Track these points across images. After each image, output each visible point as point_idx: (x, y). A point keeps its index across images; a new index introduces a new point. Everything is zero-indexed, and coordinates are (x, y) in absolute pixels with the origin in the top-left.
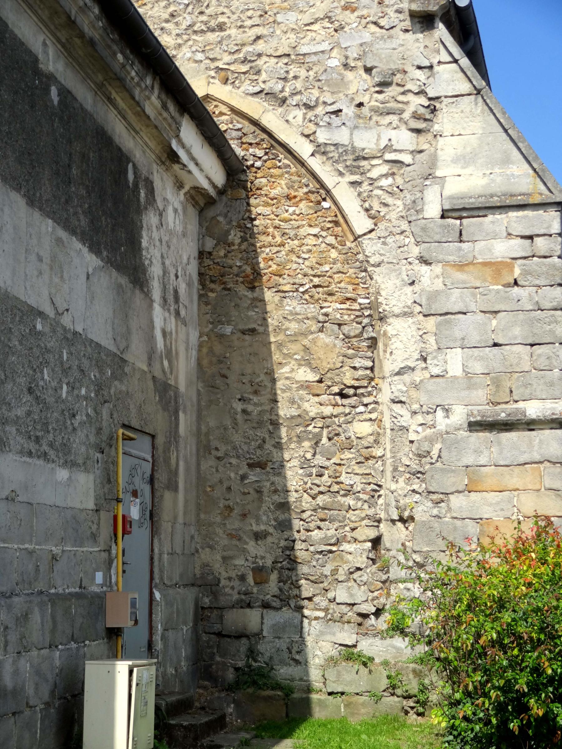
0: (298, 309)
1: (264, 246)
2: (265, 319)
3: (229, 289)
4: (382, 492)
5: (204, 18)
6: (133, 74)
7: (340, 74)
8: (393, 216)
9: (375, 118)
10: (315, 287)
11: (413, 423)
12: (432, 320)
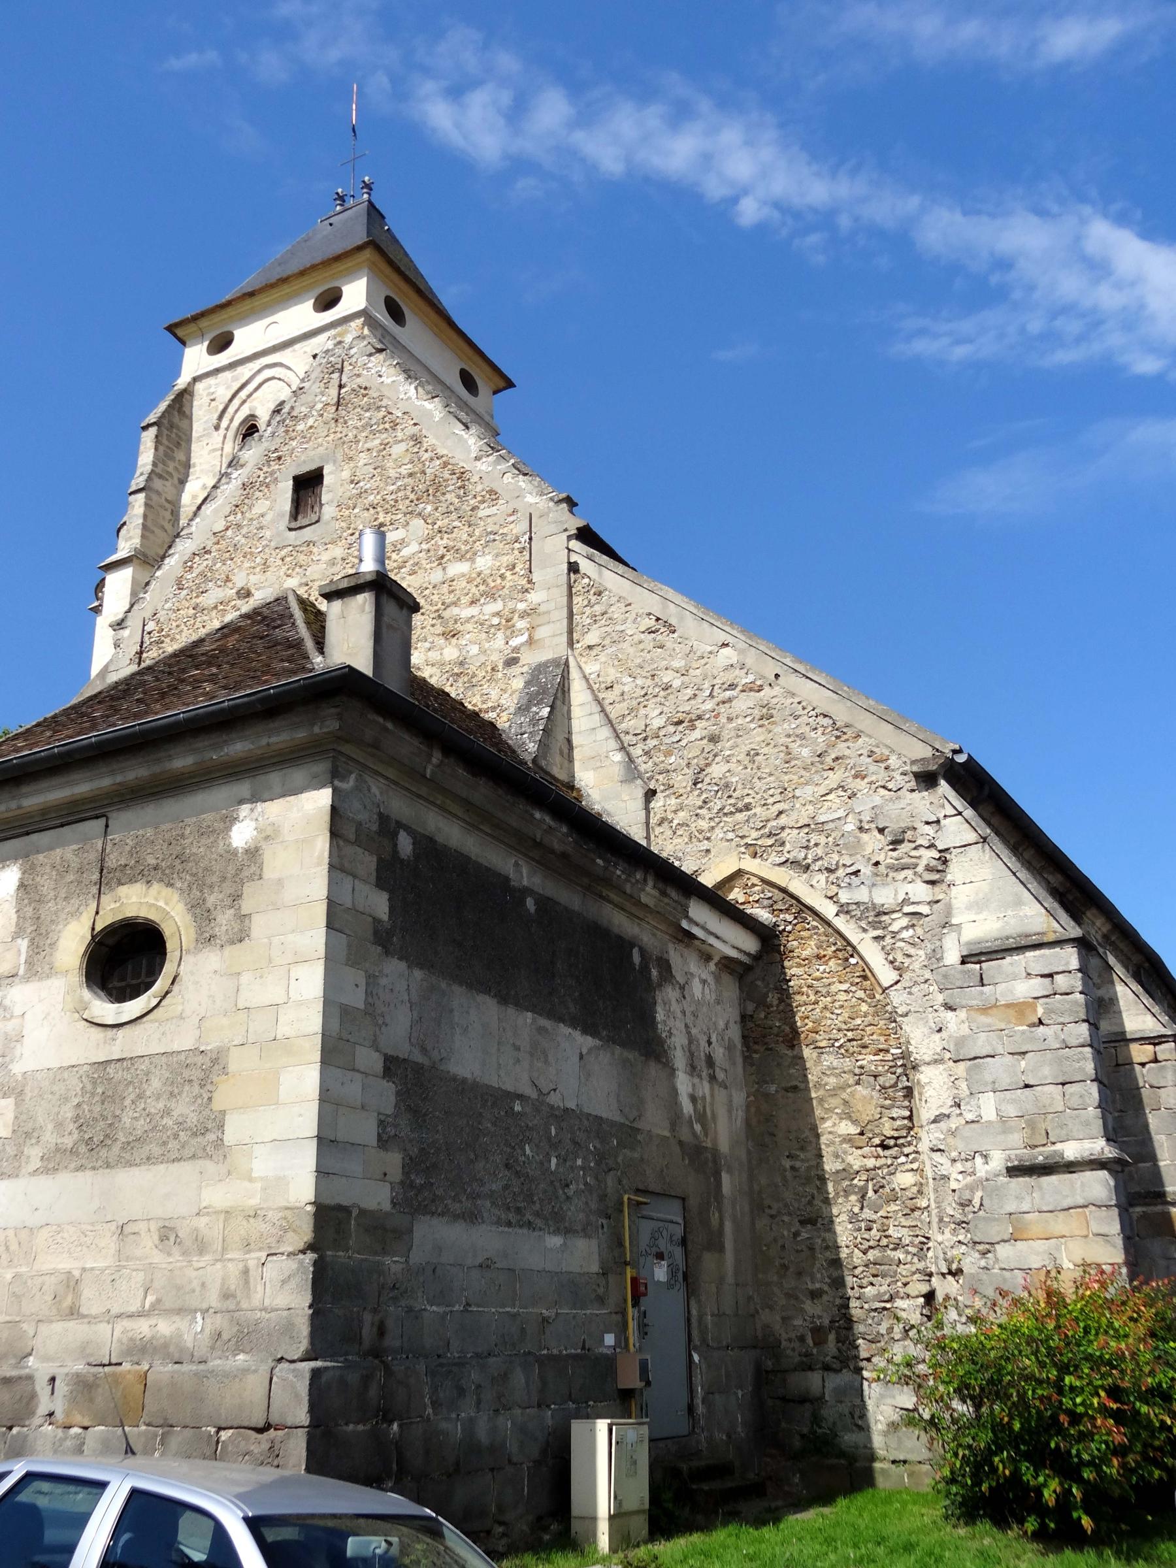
0: (835, 1064)
1: (800, 1005)
2: (805, 1076)
3: (771, 1049)
4: (930, 1244)
5: (732, 801)
6: (618, 872)
7: (856, 837)
8: (916, 966)
9: (891, 874)
10: (849, 1040)
11: (954, 1171)
12: (962, 1066)
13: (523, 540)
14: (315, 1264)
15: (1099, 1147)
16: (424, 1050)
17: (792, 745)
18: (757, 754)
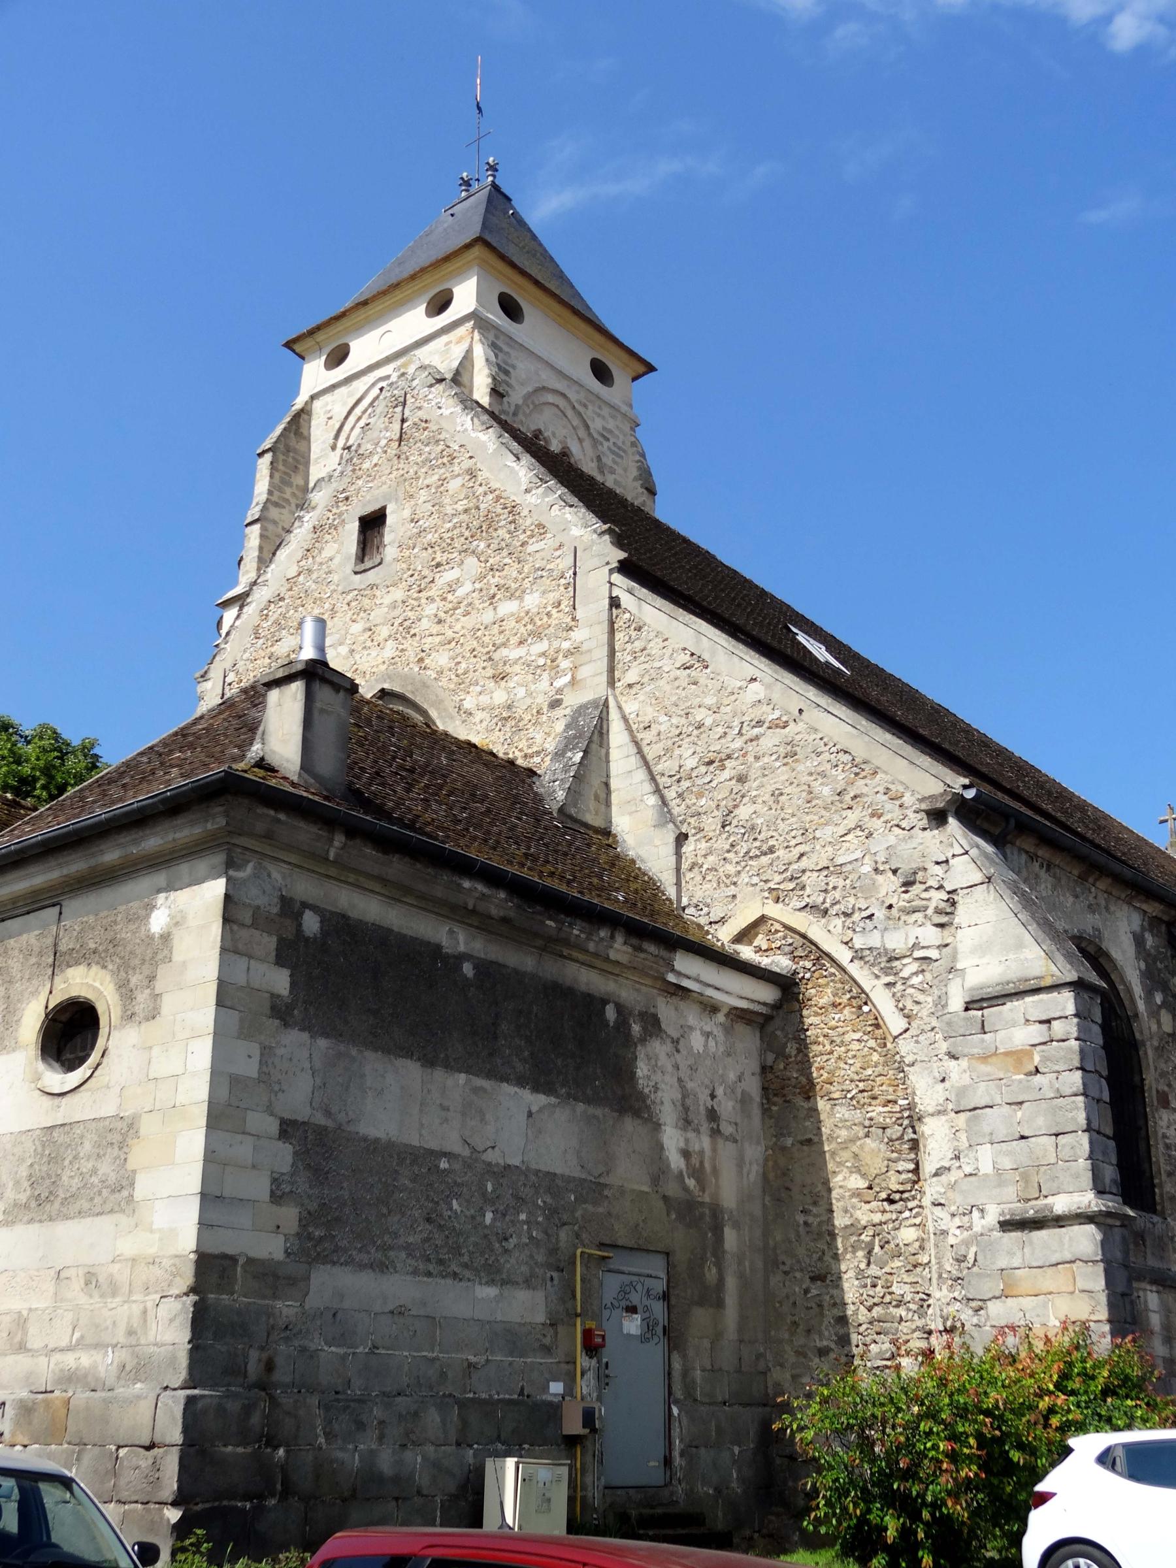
0: (846, 1116)
1: (816, 1056)
2: (819, 1129)
3: (788, 1102)
4: (931, 1301)
5: (757, 844)
6: (576, 932)
8: (924, 1013)
9: (903, 918)
10: (862, 1091)
11: (951, 1225)
12: (963, 1117)
13: (567, 575)
14: (195, 1304)
15: (1088, 1200)
16: (328, 1113)
17: (814, 784)
18: (782, 794)
